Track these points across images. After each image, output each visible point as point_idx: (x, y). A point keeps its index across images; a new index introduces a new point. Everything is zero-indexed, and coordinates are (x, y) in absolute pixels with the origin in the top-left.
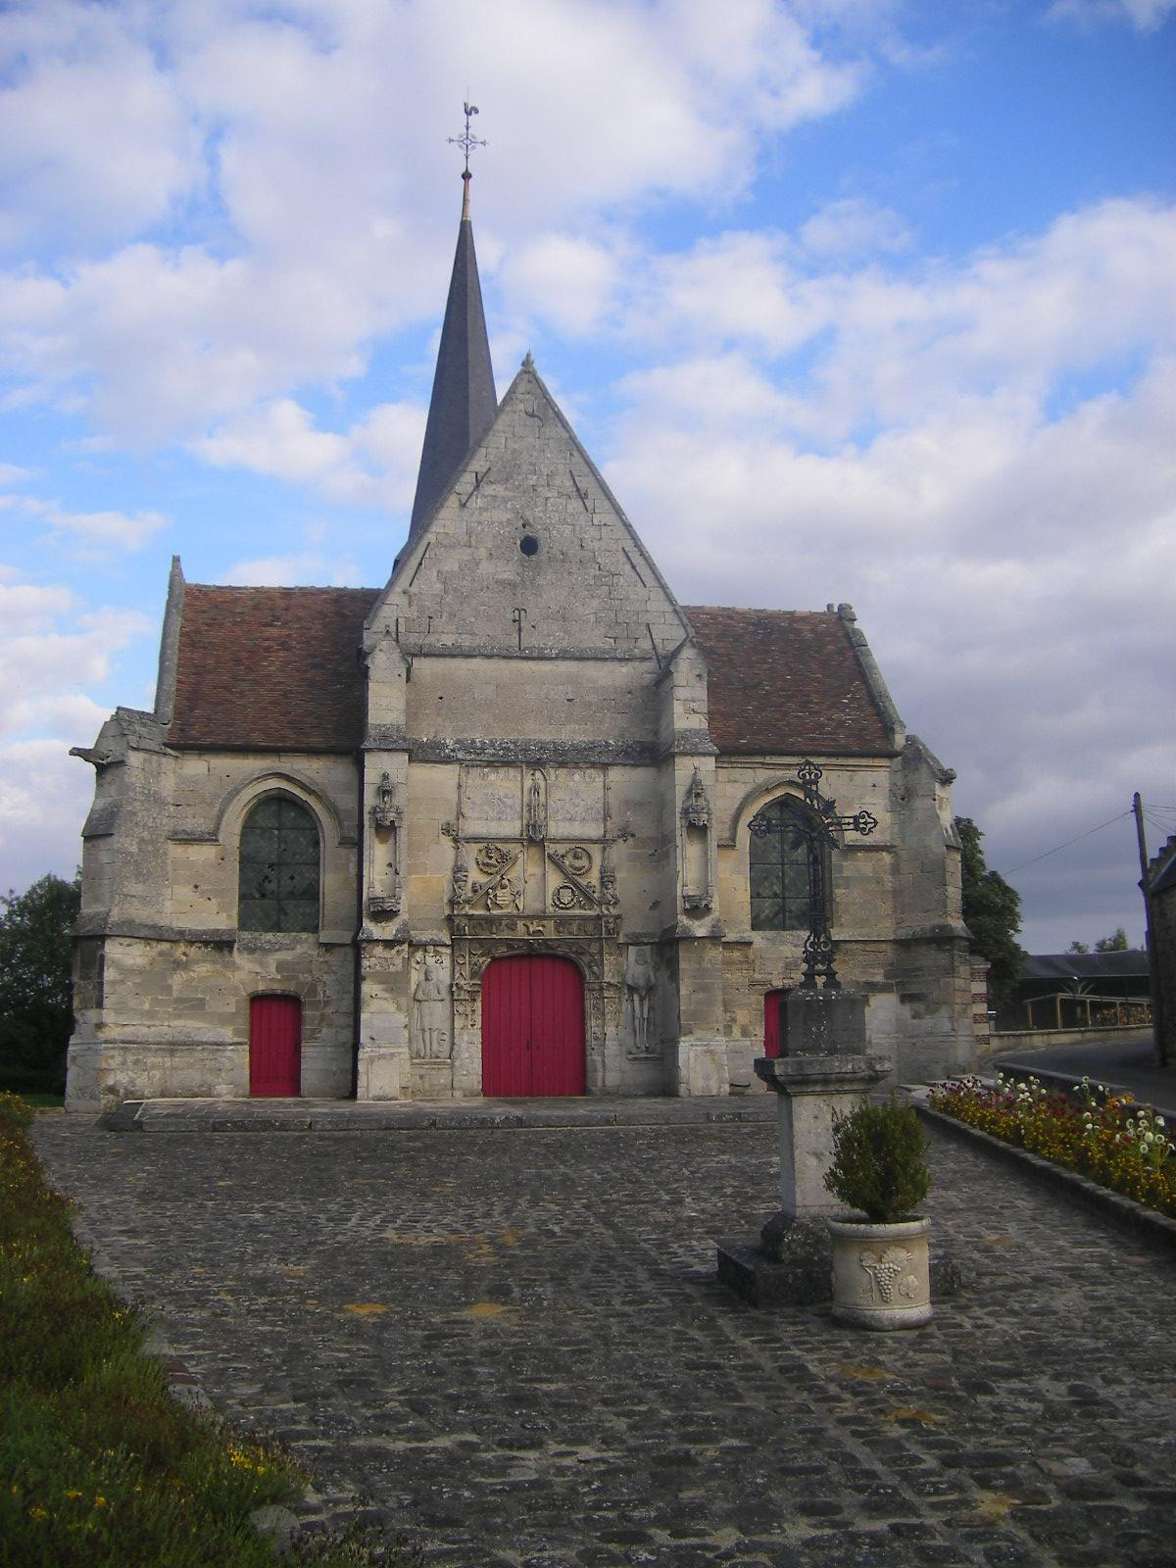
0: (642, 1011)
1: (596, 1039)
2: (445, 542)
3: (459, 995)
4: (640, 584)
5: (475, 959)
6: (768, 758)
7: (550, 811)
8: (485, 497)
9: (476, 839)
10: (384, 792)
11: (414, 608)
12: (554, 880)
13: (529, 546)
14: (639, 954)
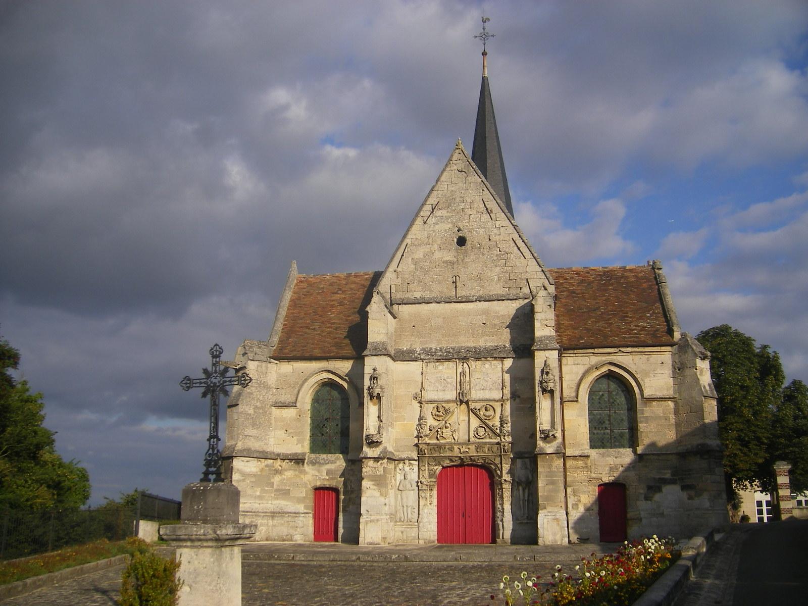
2: (416, 243)
3: (422, 487)
6: (596, 350)
8: (436, 217)
9: (431, 402)
10: (374, 378)
11: (400, 279)
12: (475, 422)
13: (462, 241)
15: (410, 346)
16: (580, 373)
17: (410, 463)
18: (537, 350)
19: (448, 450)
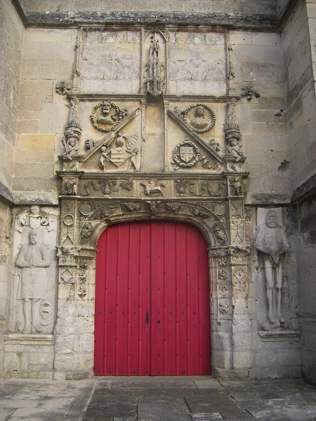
0: (275, 283)
1: (223, 312)
3: (65, 261)
5: (85, 222)
7: (169, 71)
9: (90, 97)
12: (175, 137)
14: (268, 216)
17: (41, 212)
18: (85, 376)
19: (120, 188)
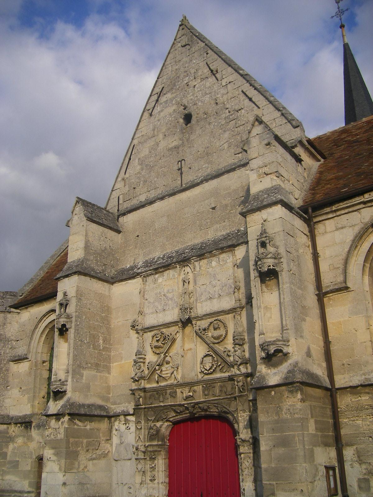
4: (256, 108)
11: (127, 186)
15: (133, 262)
16: (348, 240)
